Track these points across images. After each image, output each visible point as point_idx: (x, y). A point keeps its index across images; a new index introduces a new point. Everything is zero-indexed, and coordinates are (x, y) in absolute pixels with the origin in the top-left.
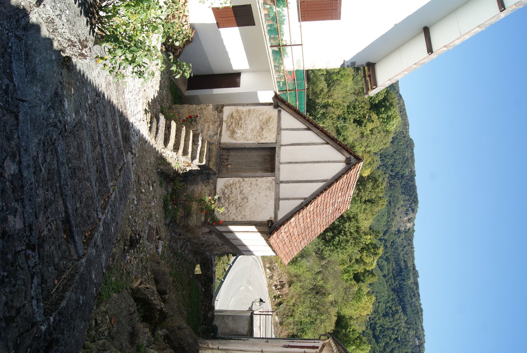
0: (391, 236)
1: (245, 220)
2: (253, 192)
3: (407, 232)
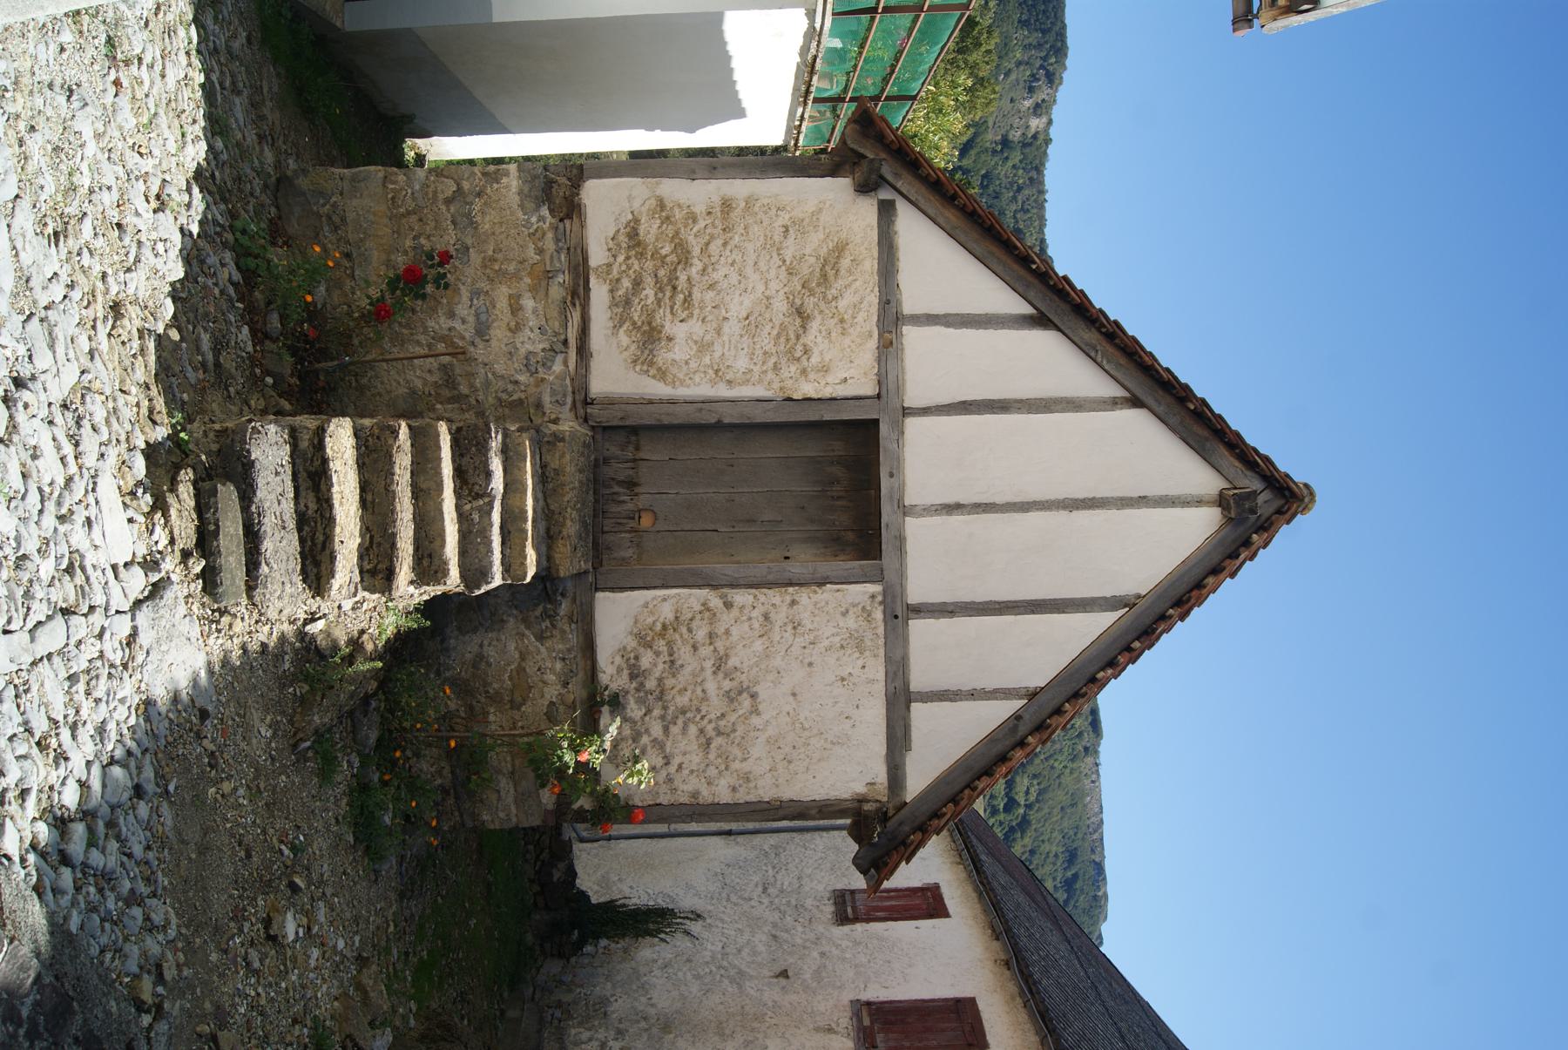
0: (983, 157)
1: (752, 798)
3: (1030, 145)
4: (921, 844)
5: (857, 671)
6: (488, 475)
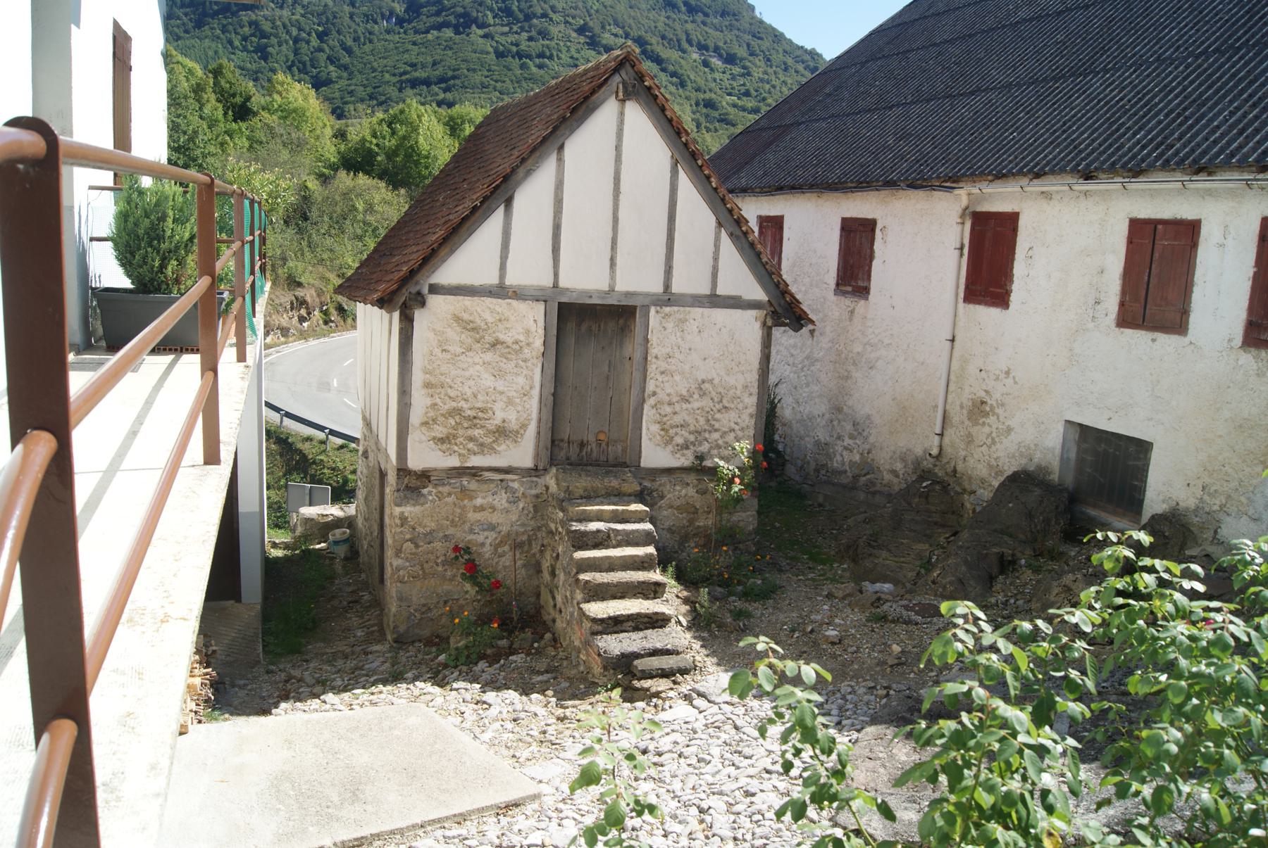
1: (756, 385)
2: (687, 367)
4: (792, 296)
5: (696, 324)
6: (598, 531)
